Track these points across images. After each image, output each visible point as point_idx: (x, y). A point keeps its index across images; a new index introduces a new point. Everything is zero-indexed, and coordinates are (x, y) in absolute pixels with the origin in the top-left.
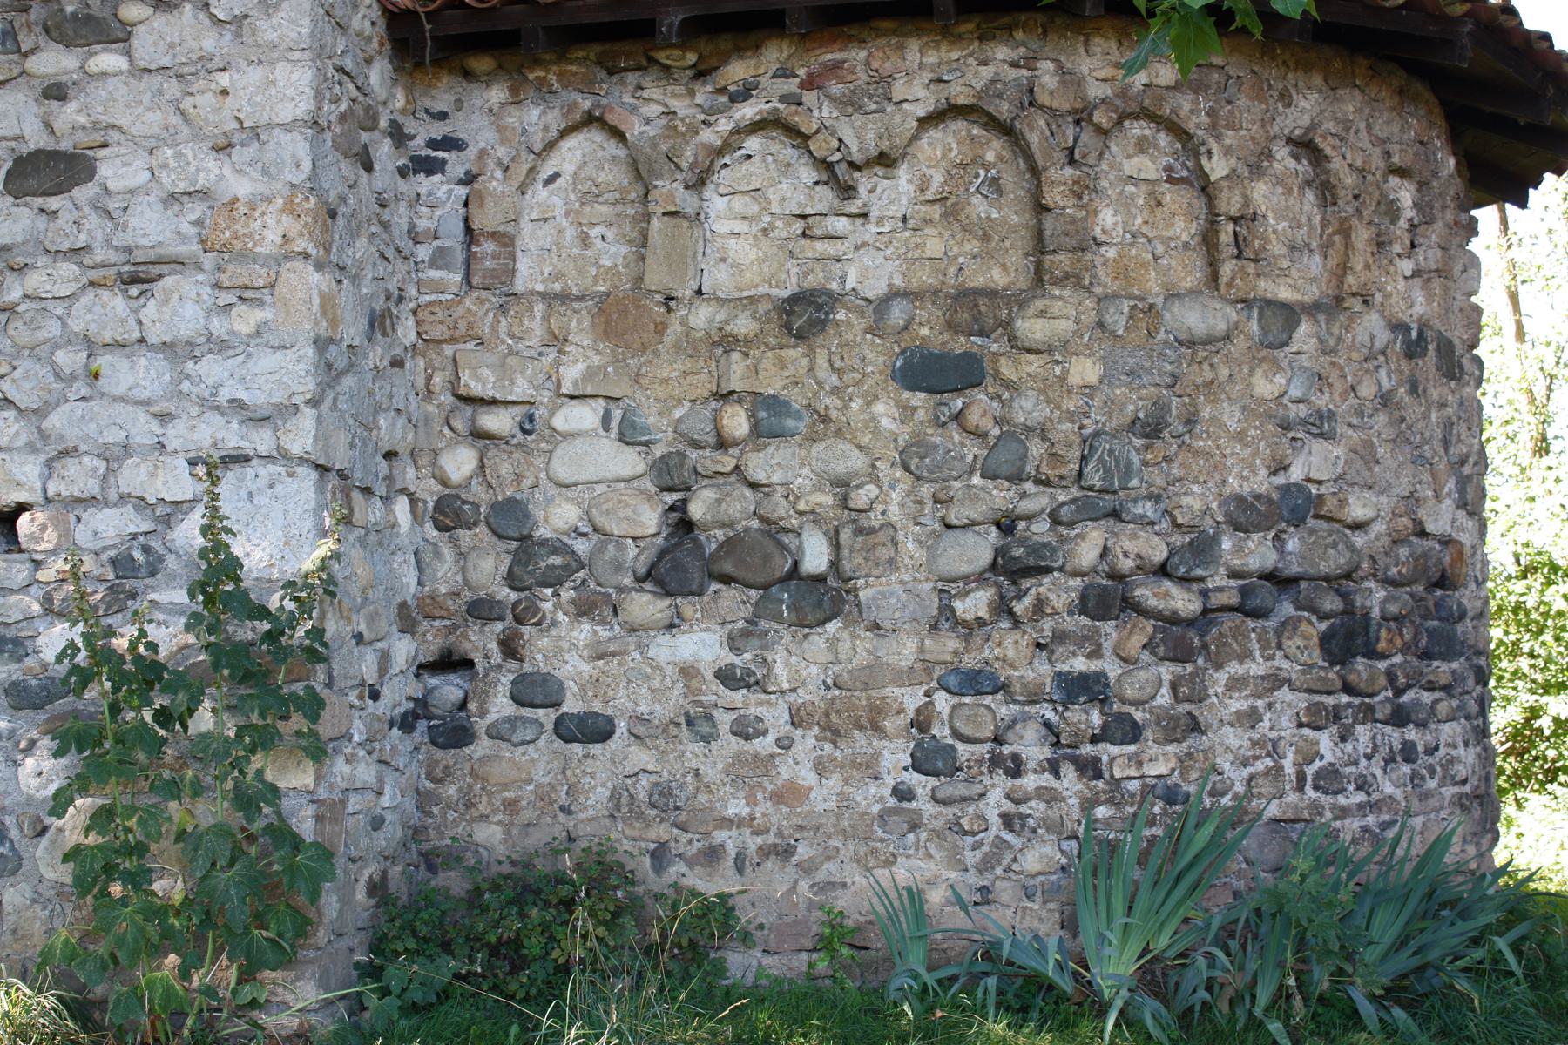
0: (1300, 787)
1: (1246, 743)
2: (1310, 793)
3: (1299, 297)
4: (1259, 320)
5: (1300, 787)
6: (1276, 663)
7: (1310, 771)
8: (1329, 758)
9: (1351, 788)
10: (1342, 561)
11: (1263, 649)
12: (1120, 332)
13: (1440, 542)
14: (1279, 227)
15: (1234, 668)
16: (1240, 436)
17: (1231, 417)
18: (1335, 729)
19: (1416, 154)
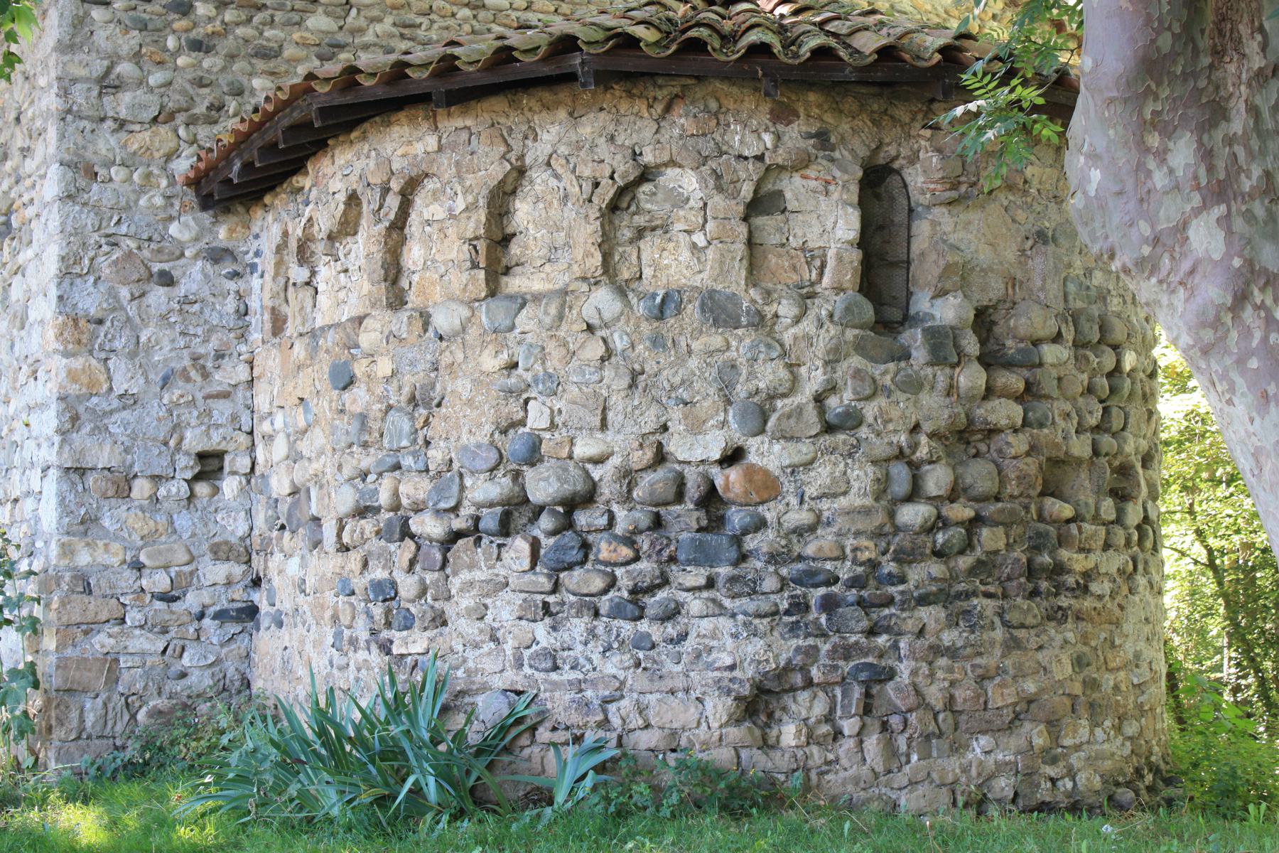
0: (519, 664)
1: (476, 631)
2: (527, 670)
3: (551, 286)
4: (487, 313)
5: (519, 664)
6: (496, 571)
7: (527, 653)
8: (544, 643)
9: (567, 667)
10: (551, 490)
11: (486, 560)
12: (404, 336)
13: (392, 510)
14: (538, 235)
15: (465, 575)
16: (470, 402)
17: (463, 386)
18: (548, 620)
19: (1225, 222)
